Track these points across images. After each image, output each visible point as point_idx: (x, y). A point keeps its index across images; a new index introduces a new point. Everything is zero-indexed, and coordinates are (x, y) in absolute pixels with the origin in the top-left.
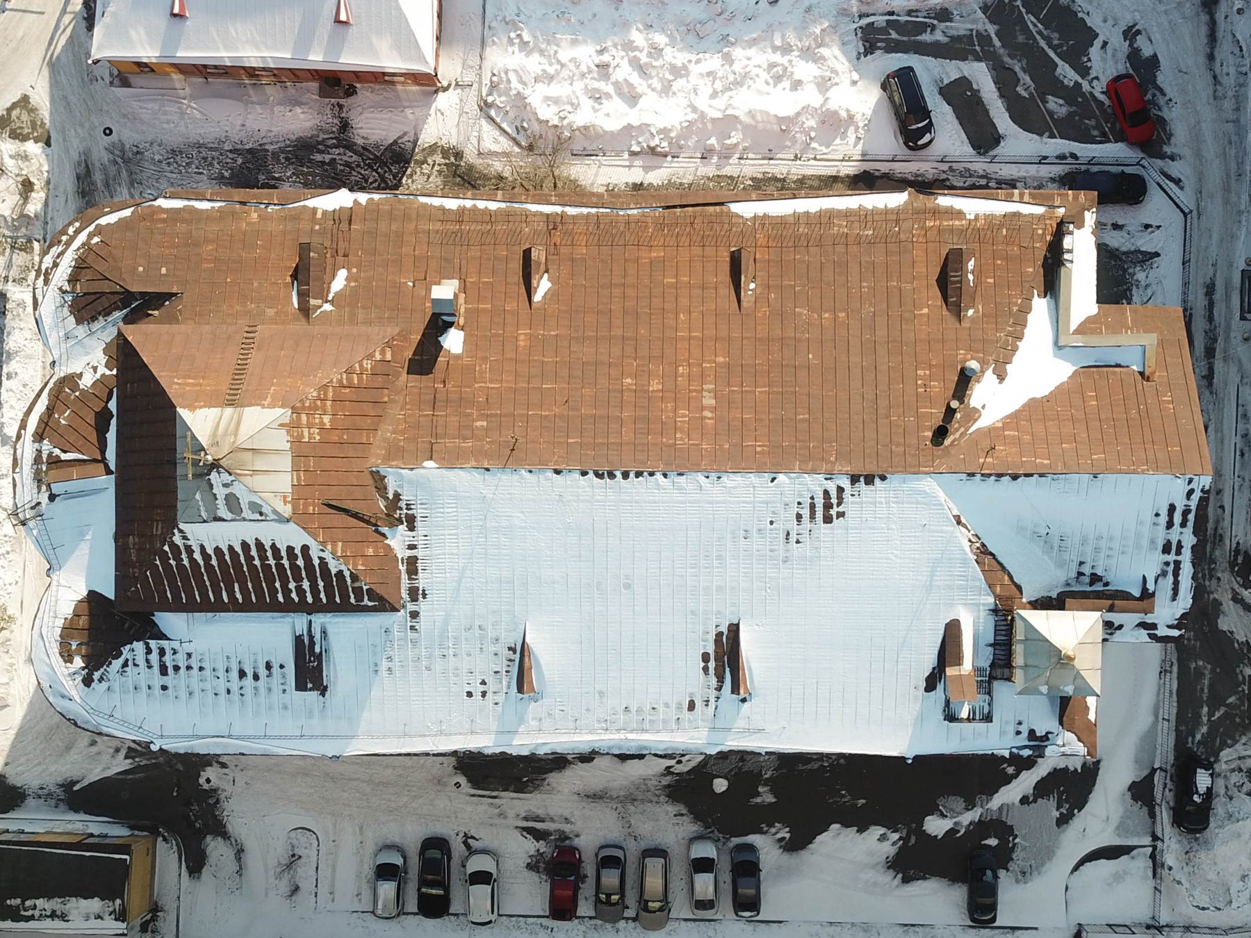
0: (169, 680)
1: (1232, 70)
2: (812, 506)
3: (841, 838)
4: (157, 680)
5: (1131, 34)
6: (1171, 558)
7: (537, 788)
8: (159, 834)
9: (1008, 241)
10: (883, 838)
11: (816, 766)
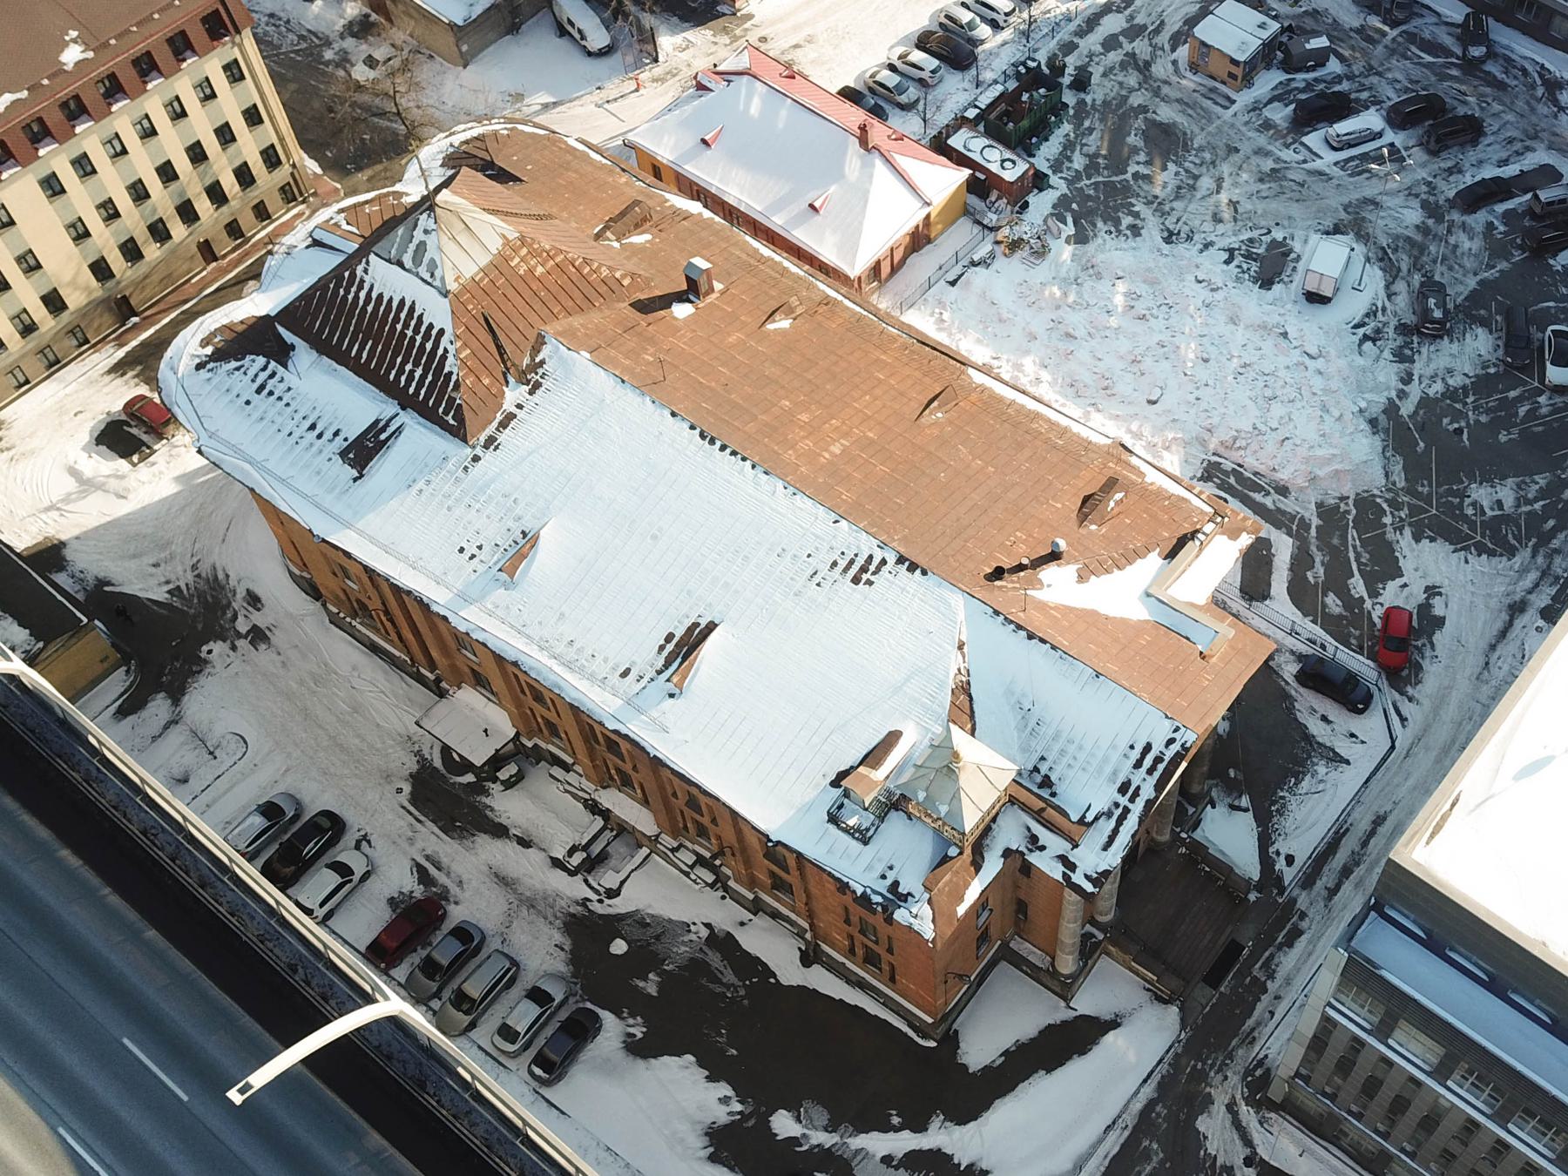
0: (256, 399)
1: (1506, 668)
2: (852, 562)
3: (686, 1073)
4: (248, 393)
5: (1432, 591)
6: (1124, 801)
7: (461, 838)
8: (128, 664)
9: (1165, 509)
10: (725, 1100)
11: (718, 990)
